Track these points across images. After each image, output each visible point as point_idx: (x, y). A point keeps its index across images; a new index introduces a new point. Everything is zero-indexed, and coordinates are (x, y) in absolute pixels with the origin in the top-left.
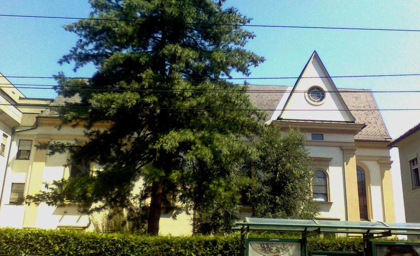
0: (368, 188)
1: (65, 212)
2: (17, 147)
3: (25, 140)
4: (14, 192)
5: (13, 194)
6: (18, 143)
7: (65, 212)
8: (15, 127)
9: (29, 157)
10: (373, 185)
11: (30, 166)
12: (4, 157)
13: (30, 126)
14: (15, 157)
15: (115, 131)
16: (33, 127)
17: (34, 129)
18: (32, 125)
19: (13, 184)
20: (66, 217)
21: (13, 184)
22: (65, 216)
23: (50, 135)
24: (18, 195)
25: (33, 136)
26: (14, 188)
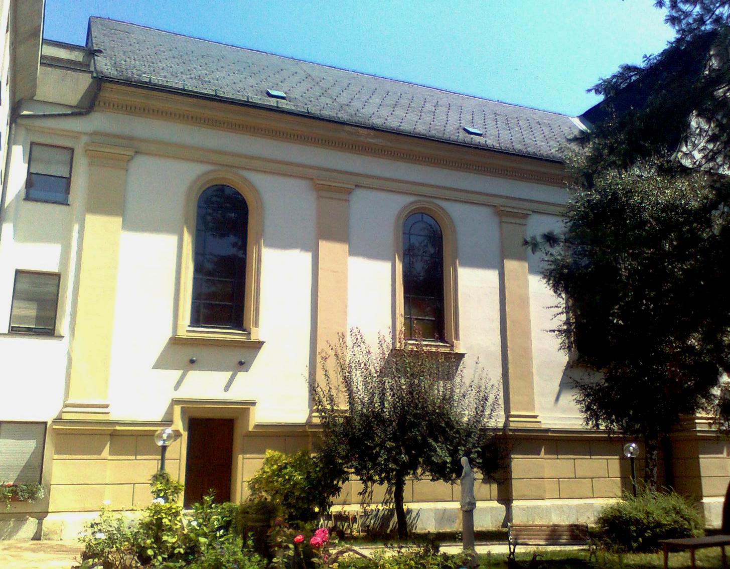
0: (448, 271)
1: (241, 363)
2: (26, 165)
3: (46, 145)
4: (24, 300)
5: (22, 304)
6: (28, 150)
7: (192, 362)
8: (22, 99)
9: (67, 199)
10: (464, 264)
11: (76, 227)
12: (69, 205)
13: (71, 107)
14: (23, 195)
15: (664, 227)
16: (77, 110)
17: (73, 114)
18: (74, 102)
19: (18, 272)
20: (194, 376)
21: (18, 272)
22: (241, 375)
23: (131, 138)
24: (35, 307)
25: (77, 135)
26: (23, 286)
